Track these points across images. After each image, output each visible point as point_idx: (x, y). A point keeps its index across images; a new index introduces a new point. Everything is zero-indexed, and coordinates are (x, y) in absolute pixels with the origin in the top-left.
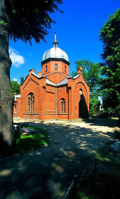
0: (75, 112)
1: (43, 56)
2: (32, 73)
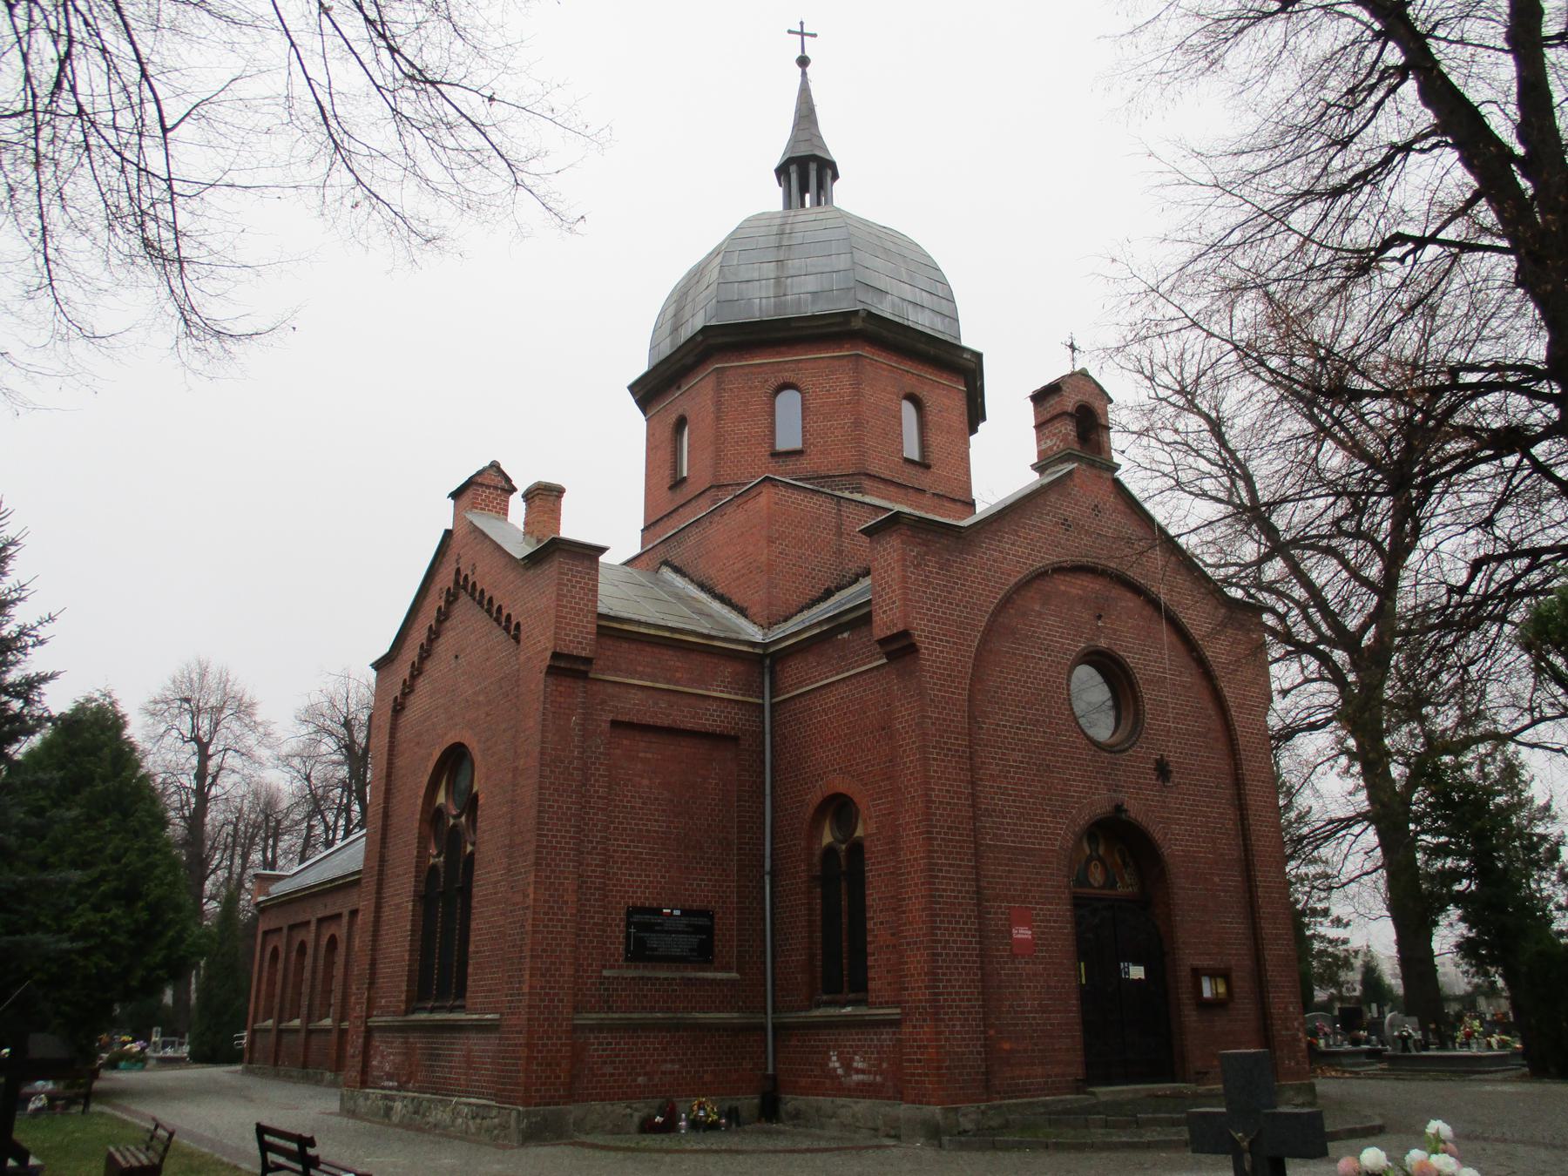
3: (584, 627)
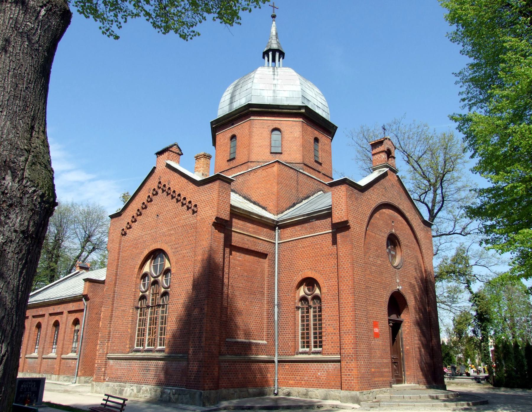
0: (370, 349)
1: (222, 100)
2: (169, 162)
3: (226, 208)
